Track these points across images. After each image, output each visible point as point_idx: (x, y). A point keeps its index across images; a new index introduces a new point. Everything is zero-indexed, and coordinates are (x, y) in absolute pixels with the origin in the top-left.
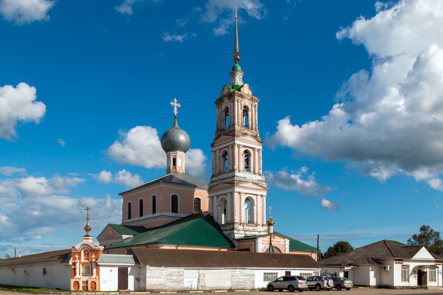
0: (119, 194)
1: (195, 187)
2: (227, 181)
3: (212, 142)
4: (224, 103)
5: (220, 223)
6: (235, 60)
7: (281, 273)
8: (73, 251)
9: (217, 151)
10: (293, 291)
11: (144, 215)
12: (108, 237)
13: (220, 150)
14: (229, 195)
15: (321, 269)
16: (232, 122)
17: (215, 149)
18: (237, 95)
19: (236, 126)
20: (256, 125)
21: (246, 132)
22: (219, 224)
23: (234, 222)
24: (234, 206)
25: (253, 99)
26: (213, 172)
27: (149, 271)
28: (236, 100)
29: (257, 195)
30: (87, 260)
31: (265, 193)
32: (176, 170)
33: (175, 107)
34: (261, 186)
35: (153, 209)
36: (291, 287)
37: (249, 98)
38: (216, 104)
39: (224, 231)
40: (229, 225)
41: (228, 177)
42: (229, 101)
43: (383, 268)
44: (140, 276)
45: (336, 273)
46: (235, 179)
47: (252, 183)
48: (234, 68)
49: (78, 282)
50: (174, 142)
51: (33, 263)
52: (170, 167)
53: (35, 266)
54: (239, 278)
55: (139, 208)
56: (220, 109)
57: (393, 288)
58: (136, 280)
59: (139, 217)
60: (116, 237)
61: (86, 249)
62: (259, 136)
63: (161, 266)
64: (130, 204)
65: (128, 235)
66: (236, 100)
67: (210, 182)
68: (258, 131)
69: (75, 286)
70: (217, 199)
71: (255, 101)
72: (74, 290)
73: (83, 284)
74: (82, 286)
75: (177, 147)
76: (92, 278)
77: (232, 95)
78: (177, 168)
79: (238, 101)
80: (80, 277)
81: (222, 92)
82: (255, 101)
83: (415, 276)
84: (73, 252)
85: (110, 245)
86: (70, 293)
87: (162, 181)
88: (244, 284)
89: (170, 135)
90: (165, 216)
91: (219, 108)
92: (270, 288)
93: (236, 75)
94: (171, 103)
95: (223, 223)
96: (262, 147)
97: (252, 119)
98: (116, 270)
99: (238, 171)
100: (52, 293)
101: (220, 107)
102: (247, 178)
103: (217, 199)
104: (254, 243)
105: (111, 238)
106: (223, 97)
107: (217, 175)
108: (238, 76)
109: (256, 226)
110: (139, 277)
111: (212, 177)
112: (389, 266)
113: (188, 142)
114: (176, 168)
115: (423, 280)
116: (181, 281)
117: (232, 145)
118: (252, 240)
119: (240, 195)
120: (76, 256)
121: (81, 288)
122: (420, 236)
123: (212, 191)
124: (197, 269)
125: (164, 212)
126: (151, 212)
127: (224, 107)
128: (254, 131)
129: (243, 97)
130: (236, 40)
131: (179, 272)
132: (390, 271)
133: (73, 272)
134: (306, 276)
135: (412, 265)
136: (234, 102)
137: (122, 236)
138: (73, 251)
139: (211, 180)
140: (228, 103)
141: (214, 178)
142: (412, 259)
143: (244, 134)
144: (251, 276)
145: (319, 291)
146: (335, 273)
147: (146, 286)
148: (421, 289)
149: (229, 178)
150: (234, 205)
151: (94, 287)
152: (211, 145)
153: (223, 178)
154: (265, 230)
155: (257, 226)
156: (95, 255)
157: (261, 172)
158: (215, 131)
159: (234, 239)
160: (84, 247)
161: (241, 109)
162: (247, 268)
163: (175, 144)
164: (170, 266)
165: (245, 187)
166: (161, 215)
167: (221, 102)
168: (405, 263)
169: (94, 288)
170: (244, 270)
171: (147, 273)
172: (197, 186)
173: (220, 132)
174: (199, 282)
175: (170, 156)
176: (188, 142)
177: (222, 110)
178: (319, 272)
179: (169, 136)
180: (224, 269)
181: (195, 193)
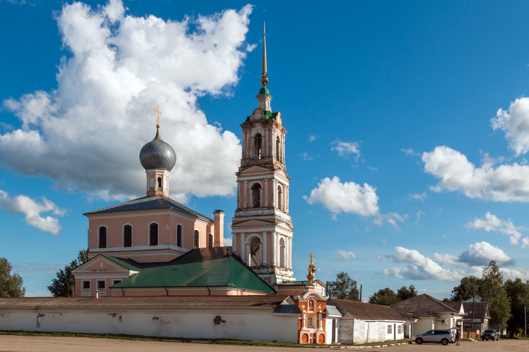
0: (83, 214)
2: (262, 218)
4: (255, 128)
6: (263, 82)
8: (300, 301)
10: (421, 344)
11: (133, 246)
12: (97, 271)
13: (284, 185)
14: (265, 235)
15: (405, 322)
17: (242, 179)
18: (275, 124)
23: (273, 266)
24: (274, 247)
26: (238, 206)
32: (163, 192)
37: (281, 129)
39: (258, 274)
43: (441, 322)
44: (342, 328)
46: (275, 218)
48: (262, 91)
49: (307, 335)
50: (163, 159)
53: (186, 312)
55: (123, 236)
56: (248, 134)
59: (124, 247)
60: (115, 272)
61: (313, 299)
64: (103, 231)
67: (235, 216)
69: (304, 338)
77: (269, 122)
78: (164, 191)
81: (252, 115)
87: (172, 208)
89: (158, 149)
92: (446, 343)
93: (266, 99)
99: (276, 209)
100: (317, 346)
101: (248, 132)
106: (254, 122)
107: (246, 210)
111: (237, 210)
113: (174, 161)
114: (162, 191)
121: (309, 342)
127: (254, 134)
129: (277, 127)
130: (264, 60)
133: (300, 324)
137: (129, 271)
138: (300, 301)
139: (235, 214)
141: (241, 212)
142: (459, 314)
147: (354, 339)
149: (266, 215)
151: (323, 340)
152: (236, 174)
153: (256, 215)
155: (287, 271)
156: (322, 306)
159: (275, 284)
160: (311, 297)
163: (164, 161)
166: (168, 248)
167: (251, 127)
169: (323, 341)
171: (354, 326)
175: (155, 174)
176: (174, 161)
179: (157, 150)
180: (378, 321)
181: (195, 224)
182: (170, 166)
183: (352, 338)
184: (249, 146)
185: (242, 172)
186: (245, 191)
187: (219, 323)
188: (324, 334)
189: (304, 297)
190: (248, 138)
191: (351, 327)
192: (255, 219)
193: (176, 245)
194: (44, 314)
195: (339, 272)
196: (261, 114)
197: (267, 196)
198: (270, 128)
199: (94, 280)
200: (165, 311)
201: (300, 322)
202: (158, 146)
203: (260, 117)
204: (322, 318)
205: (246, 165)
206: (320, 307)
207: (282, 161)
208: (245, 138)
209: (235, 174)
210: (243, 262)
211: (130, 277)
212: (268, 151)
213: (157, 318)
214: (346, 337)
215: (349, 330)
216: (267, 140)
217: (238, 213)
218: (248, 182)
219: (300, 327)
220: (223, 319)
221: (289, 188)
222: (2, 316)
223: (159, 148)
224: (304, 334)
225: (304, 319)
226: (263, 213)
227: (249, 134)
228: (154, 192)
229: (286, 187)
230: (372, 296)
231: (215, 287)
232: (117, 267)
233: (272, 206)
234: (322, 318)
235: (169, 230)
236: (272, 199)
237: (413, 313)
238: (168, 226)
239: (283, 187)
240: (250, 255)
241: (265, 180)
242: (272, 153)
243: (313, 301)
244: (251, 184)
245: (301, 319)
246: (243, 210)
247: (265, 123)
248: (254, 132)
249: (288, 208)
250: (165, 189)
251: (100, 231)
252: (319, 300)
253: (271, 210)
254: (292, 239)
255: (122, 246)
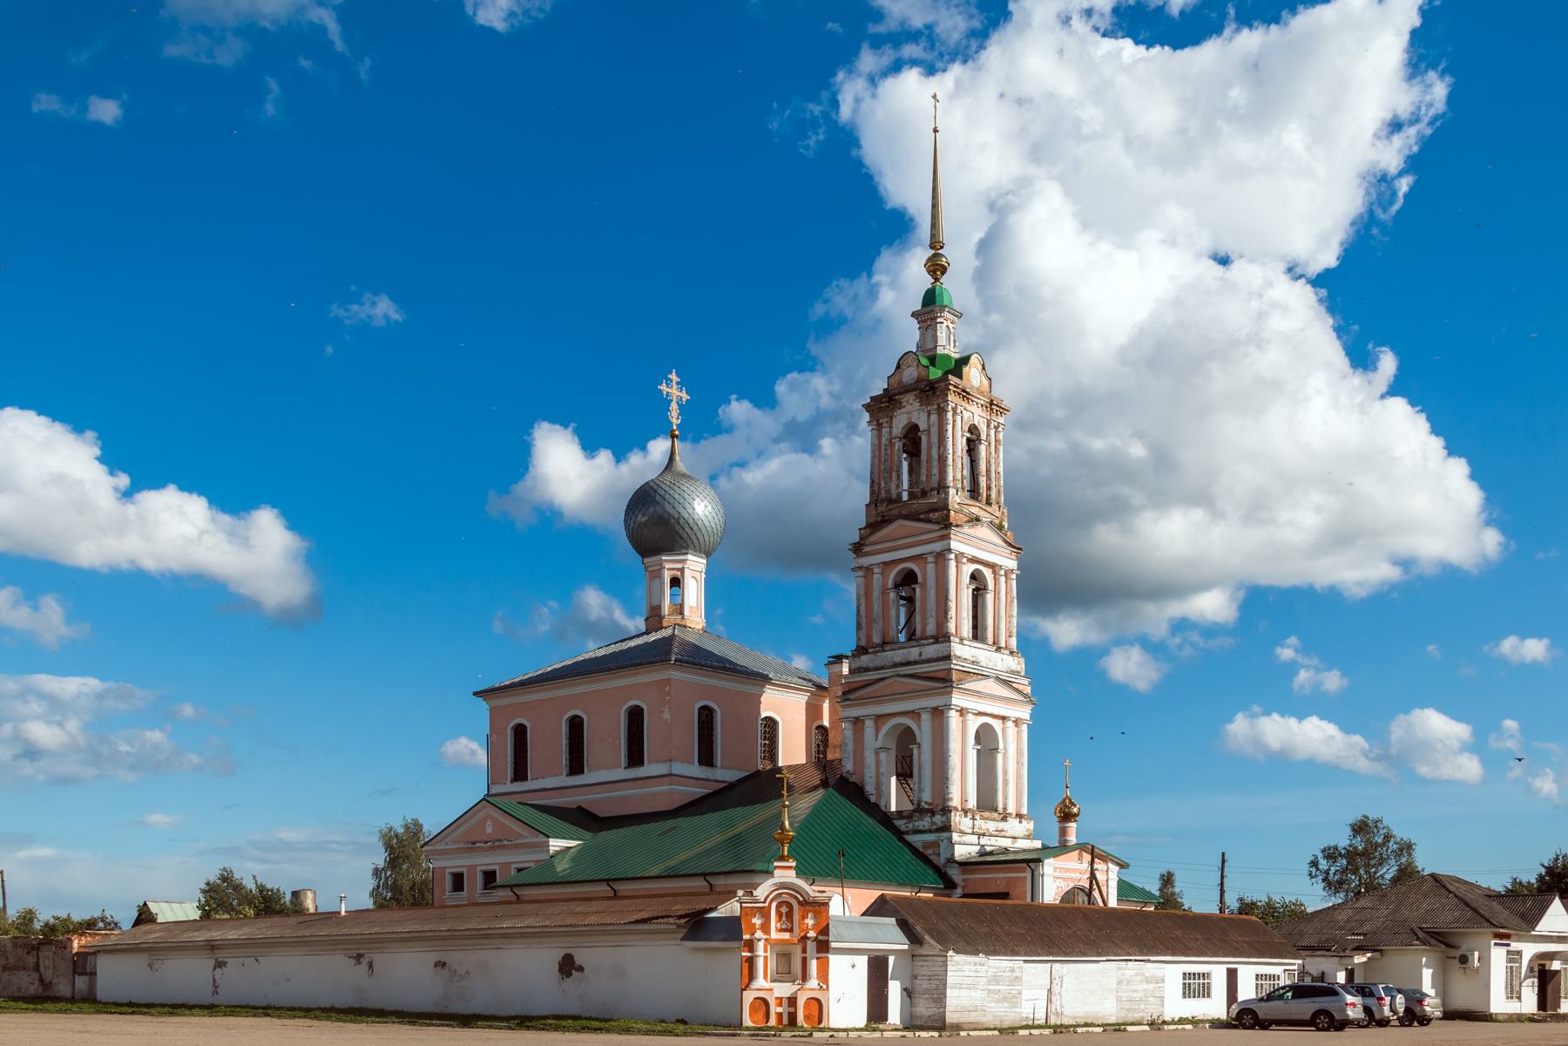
0: (475, 694)
1: (764, 679)
2: (920, 671)
3: (857, 539)
5: (886, 806)
7: (1282, 971)
9: (876, 570)
10: (1252, 1027)
12: (478, 845)
14: (925, 717)
15: (1300, 962)
16: (933, 478)
17: (866, 561)
18: (954, 392)
19: (952, 491)
20: (999, 491)
21: (975, 510)
22: (883, 809)
23: (948, 806)
24: (948, 753)
25: (995, 405)
26: (859, 639)
27: (953, 968)
28: (951, 405)
29: (1004, 718)
30: (788, 933)
31: (1024, 713)
32: (683, 618)
33: (672, 400)
34: (1017, 690)
35: (628, 751)
36: (1322, 1017)
37: (982, 402)
38: (868, 412)
39: (907, 833)
40: (929, 815)
41: (923, 657)
42: (920, 406)
43: (1457, 960)
44: (917, 982)
45: (1323, 973)
46: (952, 666)
47: (997, 678)
49: (765, 1002)
50: (679, 524)
51: (505, 936)
52: (660, 606)
54: (1133, 987)
55: (564, 746)
56: (884, 430)
57: (1489, 1018)
58: (905, 993)
59: (567, 776)
60: (516, 847)
61: (786, 898)
62: (1006, 527)
63: (975, 953)
64: (520, 732)
65: (565, 838)
66: (950, 407)
68: (1005, 511)
70: (877, 729)
71: (997, 411)
72: (752, 1025)
73: (778, 1008)
74: (776, 1013)
75: (689, 541)
76: (810, 989)
77: (936, 388)
78: (686, 612)
79: (954, 410)
80: (768, 986)
82: (997, 411)
83: (1533, 983)
84: (746, 907)
85: (519, 870)
86: (811, 1035)
88: (1142, 1007)
89: (664, 499)
90: (682, 779)
91: (880, 425)
92: (1244, 1019)
93: (938, 320)
94: (662, 388)
95: (893, 808)
96: (1016, 563)
97: (988, 471)
98: (862, 962)
99: (958, 640)
100: (746, 1033)
101: (885, 425)
102: (981, 664)
103: (877, 729)
104: (1028, 875)
105: (491, 847)
106: (900, 393)
107: (877, 649)
108: (945, 323)
109: (1004, 819)
110: (913, 983)
111: (856, 653)
112: (1476, 954)
115: (1549, 996)
116: (1014, 999)
117: (937, 553)
118: (1025, 865)
119: (961, 718)
120: (754, 921)
121: (773, 1022)
122: (1351, 854)
123: (856, 699)
124: (1047, 961)
125: (678, 763)
126: (623, 762)
127: (901, 426)
128: (995, 507)
129: (968, 399)
131: (1013, 971)
132: (1477, 970)
133: (746, 971)
134: (1201, 981)
135: (1529, 950)
136: (941, 412)
137: (548, 842)
140: (917, 413)
141: (864, 658)
142: (1533, 933)
143: (971, 521)
144: (1158, 983)
145: (1327, 1030)
146: (1320, 973)
147: (947, 1013)
148: (1559, 1022)
149: (929, 661)
150: (948, 750)
151: (816, 1014)
153: (904, 661)
154: (1027, 834)
155: (1006, 821)
156: (815, 917)
157: (1013, 643)
158: (867, 503)
161: (963, 436)
162: (1152, 958)
164: (995, 953)
165: (979, 692)
167: (891, 407)
168: (1515, 946)
169: (816, 1019)
170: (1143, 963)
171: (949, 974)
172: (772, 679)
173: (888, 505)
174: (1049, 1001)
175: (660, 569)
177: (891, 432)
178: (1295, 970)
179: (661, 501)
180: (1107, 960)
181: (762, 699)
182: (702, 542)
183: (942, 1010)
184: (888, 464)
185: (867, 542)
186: (876, 593)
187: (569, 975)
188: (823, 1002)
189: (755, 893)
190: (883, 440)
191: (940, 978)
192: (900, 673)
193: (693, 764)
194: (226, 960)
195: (1355, 816)
196: (918, 365)
197: (932, 605)
198: (942, 405)
199: (472, 868)
200: (459, 946)
201: (746, 966)
202: (667, 489)
203: (915, 374)
204: (818, 952)
205: (879, 519)
206: (810, 922)
207: (990, 496)
208: (877, 442)
209: (850, 549)
210: (868, 801)
211: (551, 857)
212: (937, 474)
213: (444, 964)
214: (927, 1008)
215: (934, 987)
216: (935, 440)
217: (857, 659)
218: (883, 569)
219: (746, 980)
220: (578, 961)
221: (1017, 575)
222: (151, 968)
223: (667, 497)
224: (755, 999)
225: (757, 956)
226: (921, 654)
227: (888, 429)
228: (661, 617)
229: (1002, 572)
230: (1506, 887)
231: (724, 876)
232: (521, 832)
233: (945, 632)
234: (818, 952)
235: (669, 722)
236: (946, 613)
237: (1365, 935)
238: (667, 710)
239: (994, 573)
240: (893, 779)
241: (926, 558)
242: (947, 476)
243: (792, 906)
244: (893, 574)
245: (749, 957)
246: (870, 651)
247: (927, 391)
248: (900, 423)
249: (1015, 634)
250: (691, 607)
251: (515, 737)
252: (806, 901)
253: (942, 645)
254: (1028, 725)
255: (562, 774)
